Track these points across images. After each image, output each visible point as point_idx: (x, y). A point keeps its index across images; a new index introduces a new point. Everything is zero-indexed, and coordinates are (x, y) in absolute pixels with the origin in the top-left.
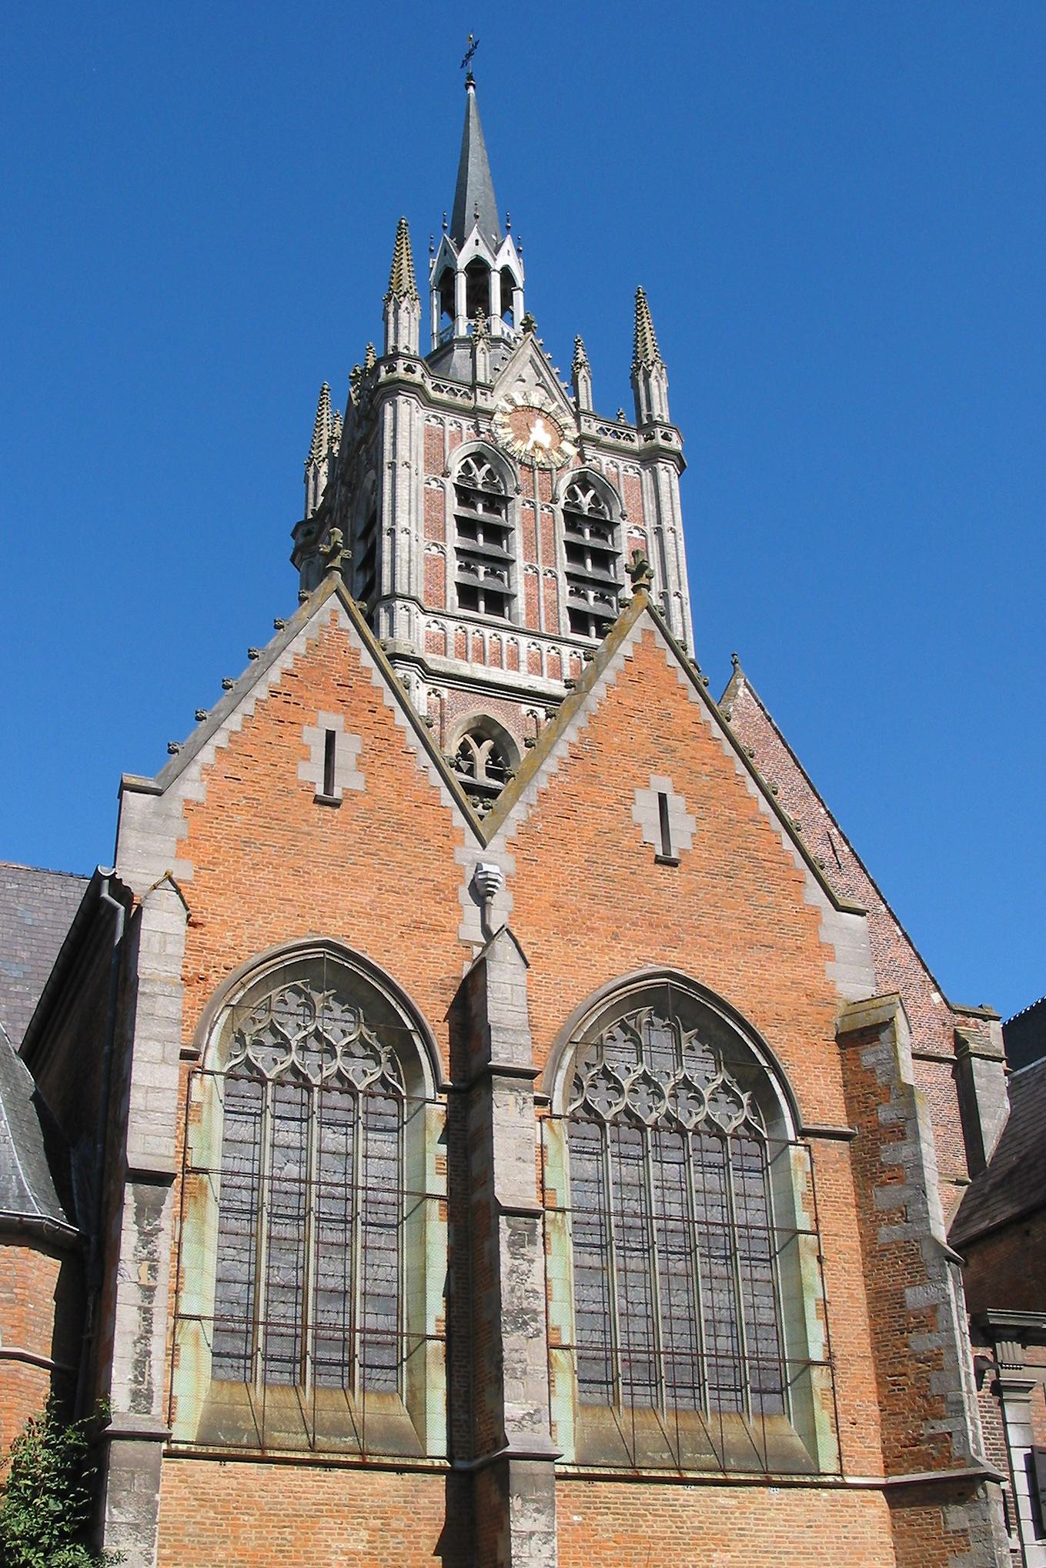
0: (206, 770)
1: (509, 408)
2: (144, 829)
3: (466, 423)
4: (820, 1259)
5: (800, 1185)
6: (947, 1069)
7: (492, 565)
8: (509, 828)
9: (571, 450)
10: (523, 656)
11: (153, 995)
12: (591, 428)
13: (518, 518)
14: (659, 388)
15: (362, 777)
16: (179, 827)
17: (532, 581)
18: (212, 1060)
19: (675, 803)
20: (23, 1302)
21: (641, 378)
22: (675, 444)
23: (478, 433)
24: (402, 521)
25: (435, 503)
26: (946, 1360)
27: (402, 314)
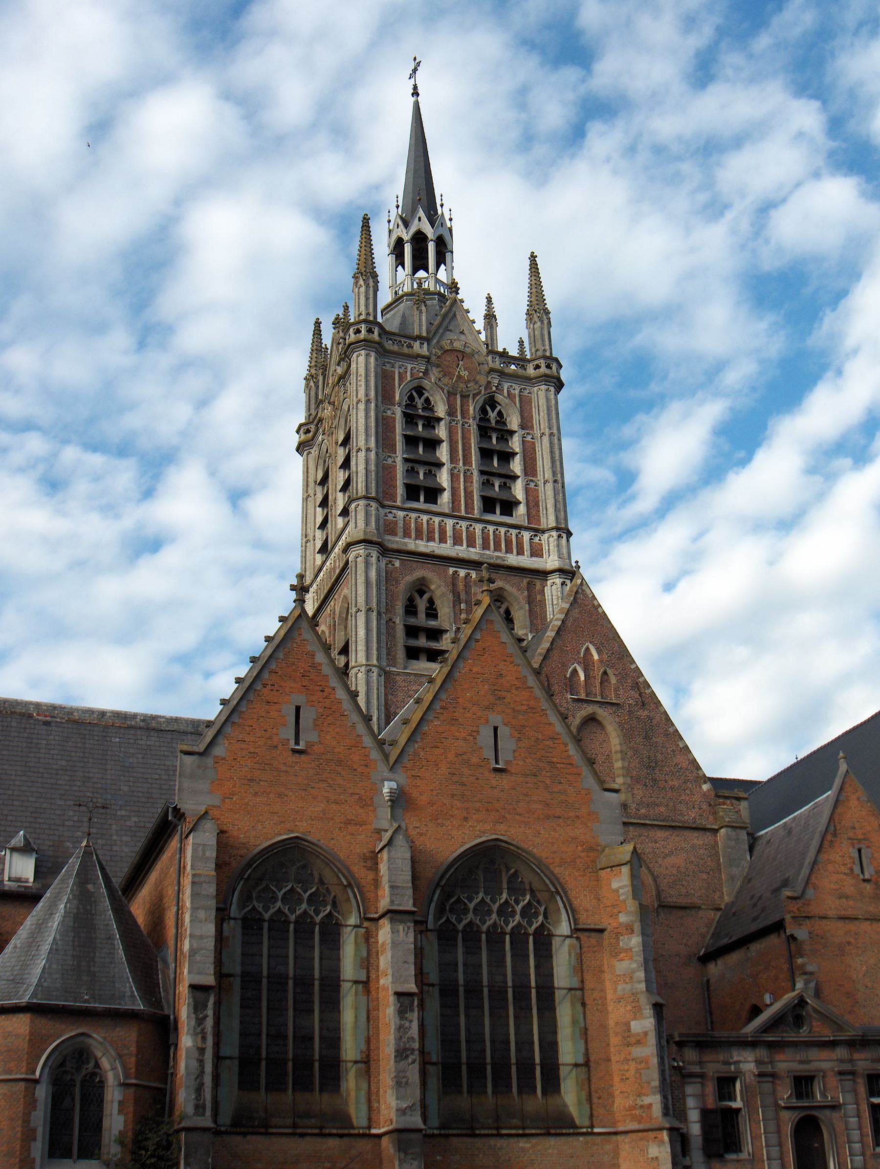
7: (428, 468)
17: (454, 477)
18: (234, 911)
19: (503, 731)
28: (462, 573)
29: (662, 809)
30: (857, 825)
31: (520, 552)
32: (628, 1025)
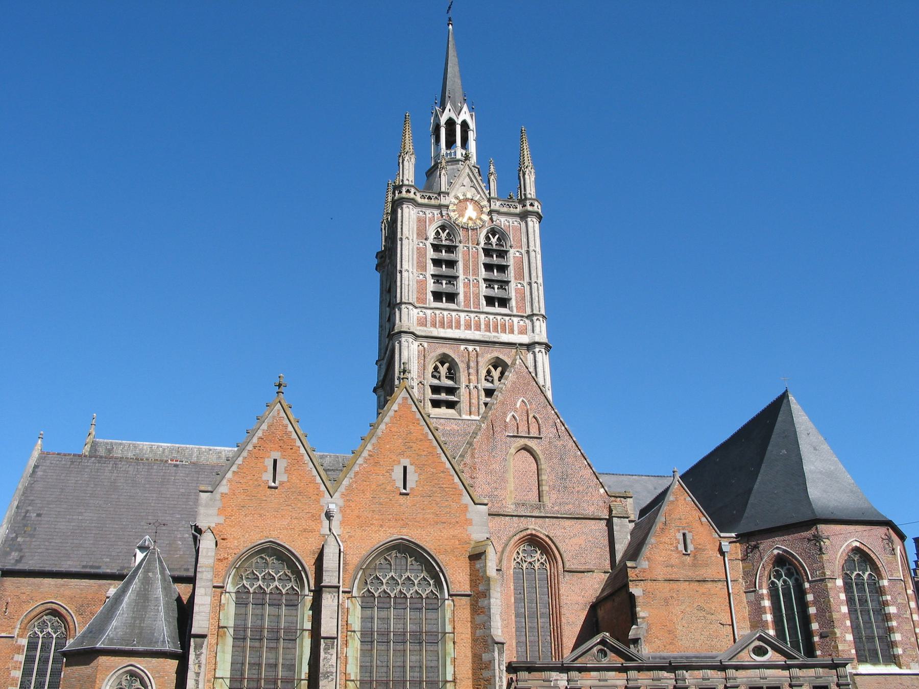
0: (229, 481)
1: (456, 201)
2: (207, 506)
3: (436, 212)
4: (454, 643)
5: (448, 615)
6: (604, 523)
8: (342, 489)
9: (485, 217)
10: (462, 322)
11: (202, 572)
12: (496, 205)
13: (460, 255)
14: (530, 179)
15: (286, 476)
16: (219, 504)
17: (467, 285)
18: (230, 587)
20: (163, 677)
21: (521, 175)
22: (537, 207)
23: (442, 216)
24: (405, 266)
25: (421, 253)
26: (492, 681)
27: (406, 163)
28: (471, 348)
29: (570, 506)
30: (683, 517)
31: (512, 332)
32: (481, 656)
